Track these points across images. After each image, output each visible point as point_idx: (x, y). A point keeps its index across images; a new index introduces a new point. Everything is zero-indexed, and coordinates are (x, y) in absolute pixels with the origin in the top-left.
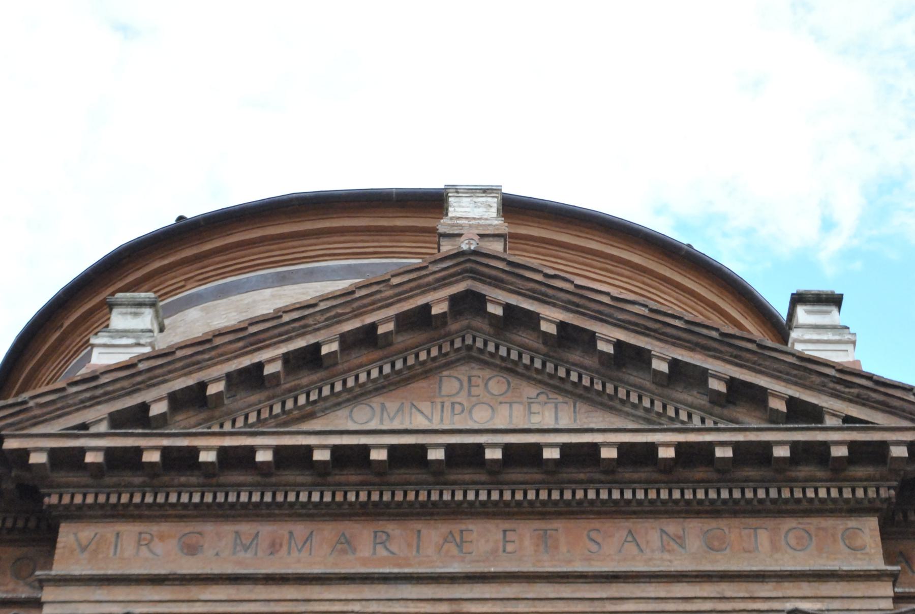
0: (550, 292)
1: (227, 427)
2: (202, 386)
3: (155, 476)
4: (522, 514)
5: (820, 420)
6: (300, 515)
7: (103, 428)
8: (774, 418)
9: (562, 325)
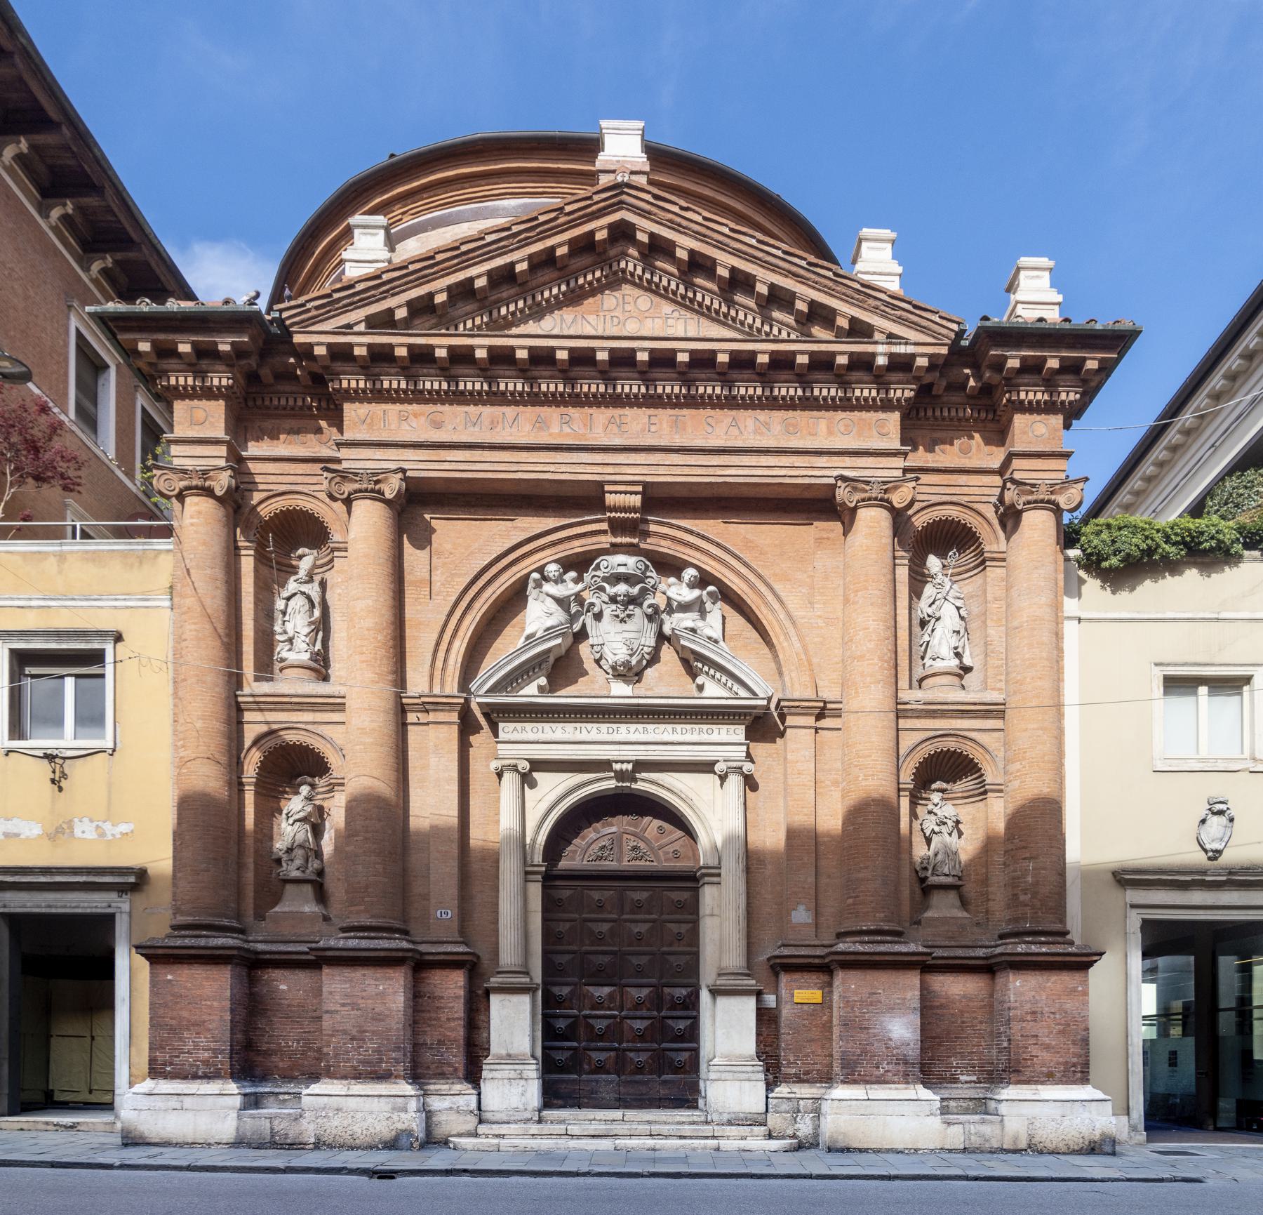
0: (684, 223)
5: (871, 336)
7: (362, 327)
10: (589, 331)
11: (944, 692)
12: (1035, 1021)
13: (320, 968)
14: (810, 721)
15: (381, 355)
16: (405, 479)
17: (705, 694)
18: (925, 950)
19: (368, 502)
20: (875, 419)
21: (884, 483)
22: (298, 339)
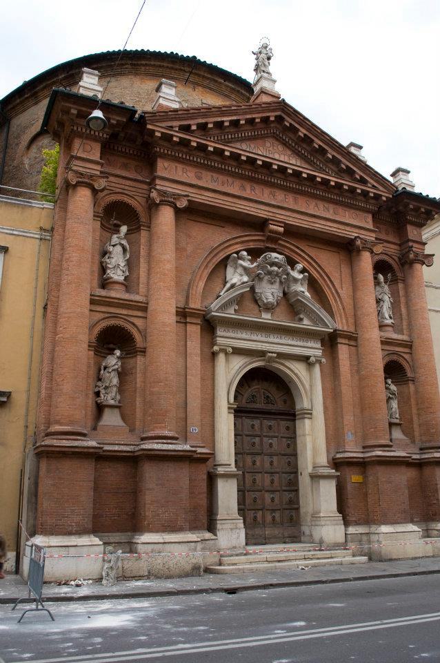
1: (212, 139)
2: (206, 124)
3: (190, 150)
7: (369, 185)
8: (355, 180)
9: (305, 135)
11: (117, 293)
15: (184, 143)
16: (189, 201)
18: (98, 446)
22: (149, 127)
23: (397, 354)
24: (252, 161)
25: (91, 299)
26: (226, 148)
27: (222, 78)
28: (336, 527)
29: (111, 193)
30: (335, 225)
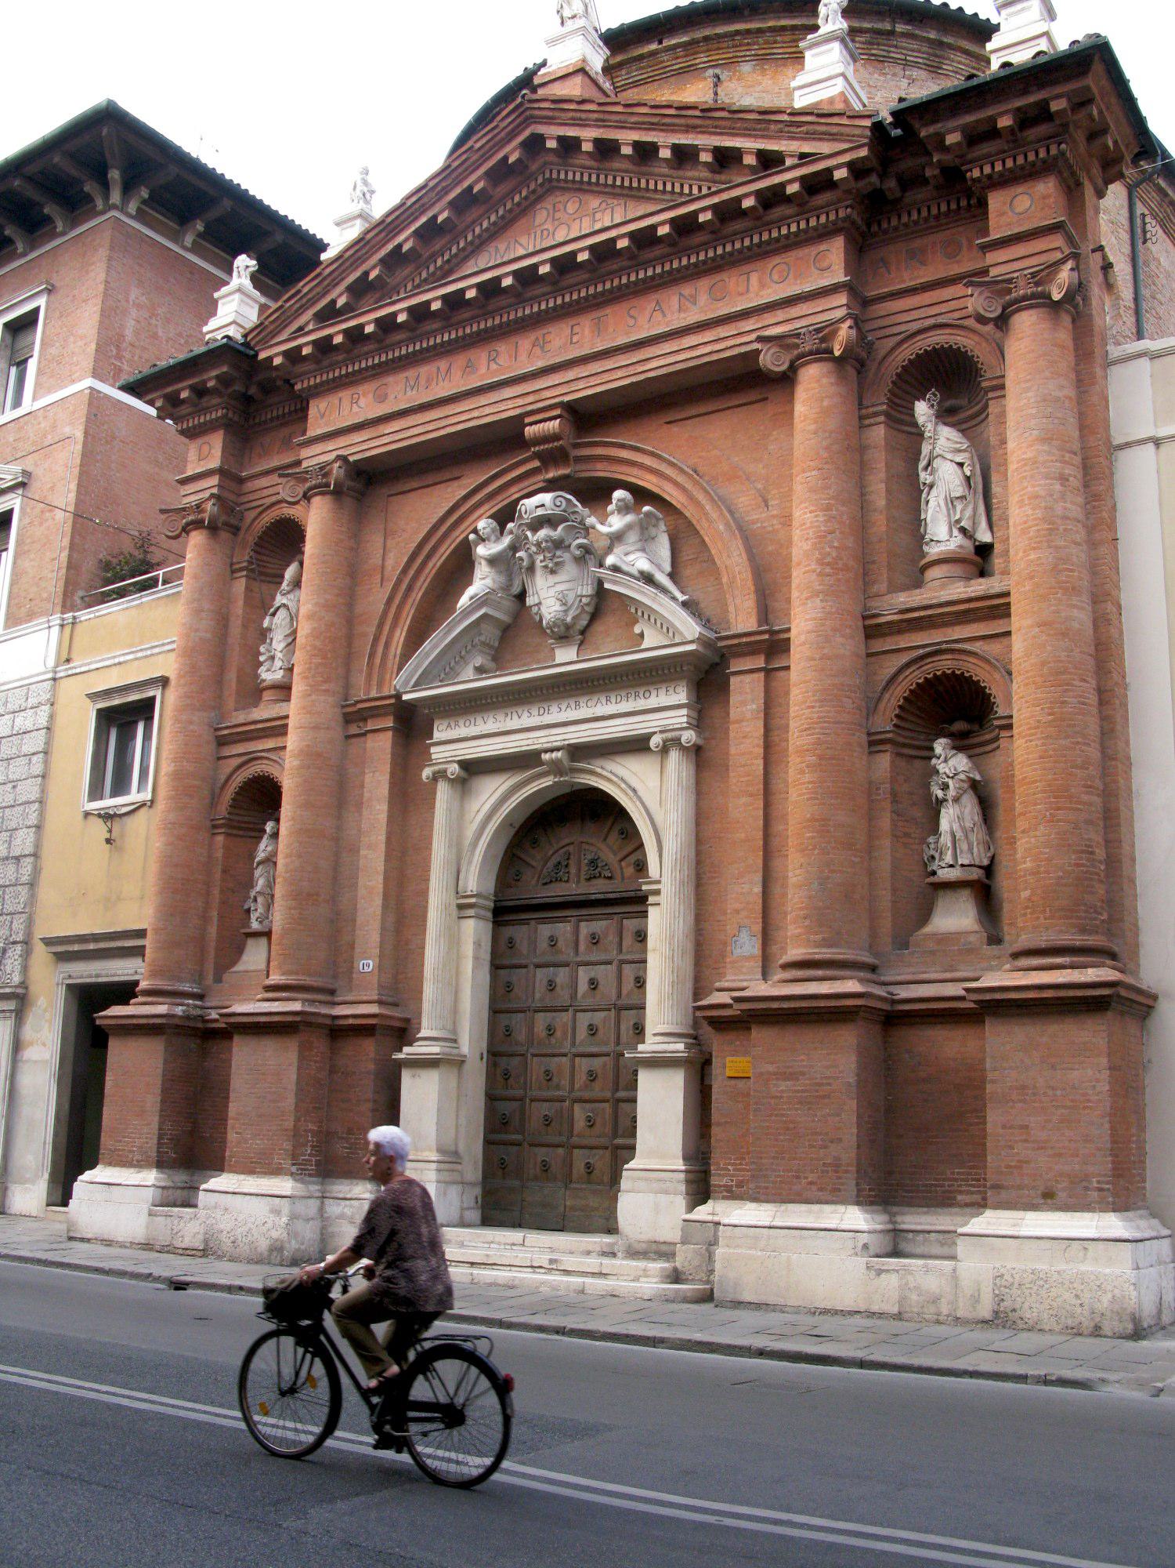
0: (584, 116)
4: (583, 309)
5: (783, 163)
6: (442, 353)
10: (521, 252)
12: (1024, 1101)
13: (231, 1038)
14: (760, 662)
17: (645, 645)
19: (1032, 312)
20: (814, 253)
21: (818, 331)
23: (952, 651)
24: (527, 277)
25: (864, 627)
26: (362, 320)
27: (649, 41)
28: (662, 1198)
29: (261, 513)
30: (708, 336)
